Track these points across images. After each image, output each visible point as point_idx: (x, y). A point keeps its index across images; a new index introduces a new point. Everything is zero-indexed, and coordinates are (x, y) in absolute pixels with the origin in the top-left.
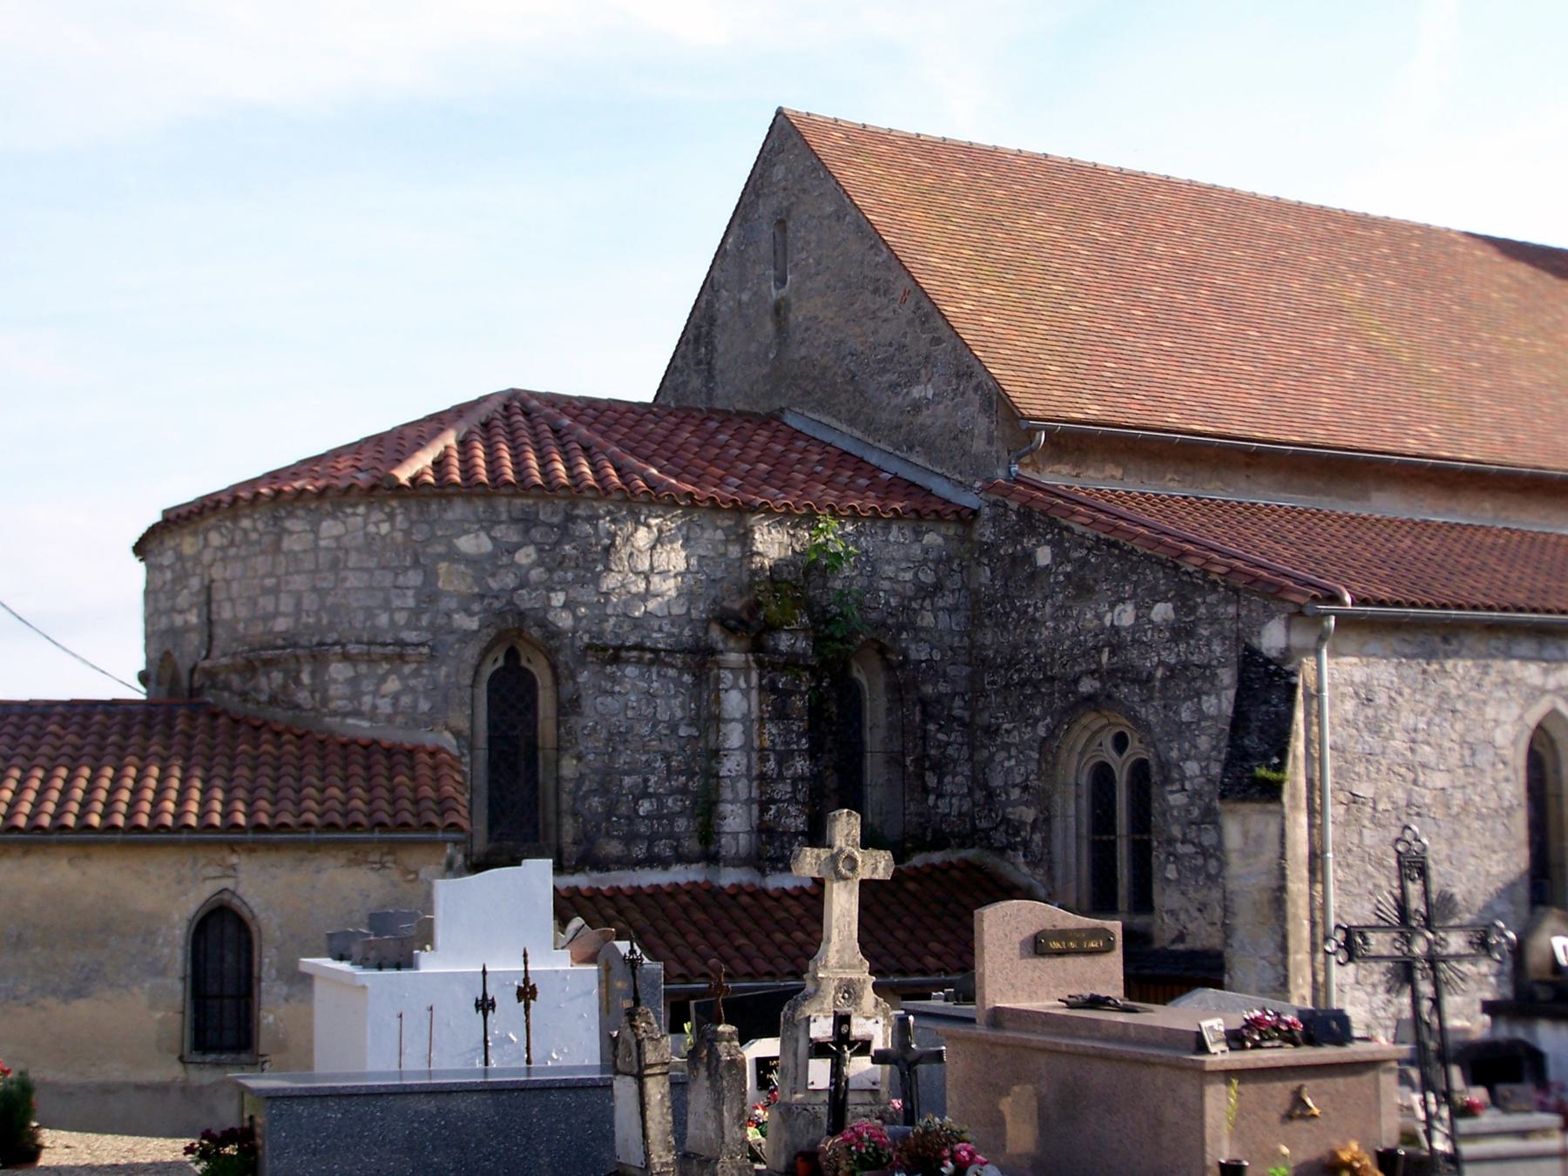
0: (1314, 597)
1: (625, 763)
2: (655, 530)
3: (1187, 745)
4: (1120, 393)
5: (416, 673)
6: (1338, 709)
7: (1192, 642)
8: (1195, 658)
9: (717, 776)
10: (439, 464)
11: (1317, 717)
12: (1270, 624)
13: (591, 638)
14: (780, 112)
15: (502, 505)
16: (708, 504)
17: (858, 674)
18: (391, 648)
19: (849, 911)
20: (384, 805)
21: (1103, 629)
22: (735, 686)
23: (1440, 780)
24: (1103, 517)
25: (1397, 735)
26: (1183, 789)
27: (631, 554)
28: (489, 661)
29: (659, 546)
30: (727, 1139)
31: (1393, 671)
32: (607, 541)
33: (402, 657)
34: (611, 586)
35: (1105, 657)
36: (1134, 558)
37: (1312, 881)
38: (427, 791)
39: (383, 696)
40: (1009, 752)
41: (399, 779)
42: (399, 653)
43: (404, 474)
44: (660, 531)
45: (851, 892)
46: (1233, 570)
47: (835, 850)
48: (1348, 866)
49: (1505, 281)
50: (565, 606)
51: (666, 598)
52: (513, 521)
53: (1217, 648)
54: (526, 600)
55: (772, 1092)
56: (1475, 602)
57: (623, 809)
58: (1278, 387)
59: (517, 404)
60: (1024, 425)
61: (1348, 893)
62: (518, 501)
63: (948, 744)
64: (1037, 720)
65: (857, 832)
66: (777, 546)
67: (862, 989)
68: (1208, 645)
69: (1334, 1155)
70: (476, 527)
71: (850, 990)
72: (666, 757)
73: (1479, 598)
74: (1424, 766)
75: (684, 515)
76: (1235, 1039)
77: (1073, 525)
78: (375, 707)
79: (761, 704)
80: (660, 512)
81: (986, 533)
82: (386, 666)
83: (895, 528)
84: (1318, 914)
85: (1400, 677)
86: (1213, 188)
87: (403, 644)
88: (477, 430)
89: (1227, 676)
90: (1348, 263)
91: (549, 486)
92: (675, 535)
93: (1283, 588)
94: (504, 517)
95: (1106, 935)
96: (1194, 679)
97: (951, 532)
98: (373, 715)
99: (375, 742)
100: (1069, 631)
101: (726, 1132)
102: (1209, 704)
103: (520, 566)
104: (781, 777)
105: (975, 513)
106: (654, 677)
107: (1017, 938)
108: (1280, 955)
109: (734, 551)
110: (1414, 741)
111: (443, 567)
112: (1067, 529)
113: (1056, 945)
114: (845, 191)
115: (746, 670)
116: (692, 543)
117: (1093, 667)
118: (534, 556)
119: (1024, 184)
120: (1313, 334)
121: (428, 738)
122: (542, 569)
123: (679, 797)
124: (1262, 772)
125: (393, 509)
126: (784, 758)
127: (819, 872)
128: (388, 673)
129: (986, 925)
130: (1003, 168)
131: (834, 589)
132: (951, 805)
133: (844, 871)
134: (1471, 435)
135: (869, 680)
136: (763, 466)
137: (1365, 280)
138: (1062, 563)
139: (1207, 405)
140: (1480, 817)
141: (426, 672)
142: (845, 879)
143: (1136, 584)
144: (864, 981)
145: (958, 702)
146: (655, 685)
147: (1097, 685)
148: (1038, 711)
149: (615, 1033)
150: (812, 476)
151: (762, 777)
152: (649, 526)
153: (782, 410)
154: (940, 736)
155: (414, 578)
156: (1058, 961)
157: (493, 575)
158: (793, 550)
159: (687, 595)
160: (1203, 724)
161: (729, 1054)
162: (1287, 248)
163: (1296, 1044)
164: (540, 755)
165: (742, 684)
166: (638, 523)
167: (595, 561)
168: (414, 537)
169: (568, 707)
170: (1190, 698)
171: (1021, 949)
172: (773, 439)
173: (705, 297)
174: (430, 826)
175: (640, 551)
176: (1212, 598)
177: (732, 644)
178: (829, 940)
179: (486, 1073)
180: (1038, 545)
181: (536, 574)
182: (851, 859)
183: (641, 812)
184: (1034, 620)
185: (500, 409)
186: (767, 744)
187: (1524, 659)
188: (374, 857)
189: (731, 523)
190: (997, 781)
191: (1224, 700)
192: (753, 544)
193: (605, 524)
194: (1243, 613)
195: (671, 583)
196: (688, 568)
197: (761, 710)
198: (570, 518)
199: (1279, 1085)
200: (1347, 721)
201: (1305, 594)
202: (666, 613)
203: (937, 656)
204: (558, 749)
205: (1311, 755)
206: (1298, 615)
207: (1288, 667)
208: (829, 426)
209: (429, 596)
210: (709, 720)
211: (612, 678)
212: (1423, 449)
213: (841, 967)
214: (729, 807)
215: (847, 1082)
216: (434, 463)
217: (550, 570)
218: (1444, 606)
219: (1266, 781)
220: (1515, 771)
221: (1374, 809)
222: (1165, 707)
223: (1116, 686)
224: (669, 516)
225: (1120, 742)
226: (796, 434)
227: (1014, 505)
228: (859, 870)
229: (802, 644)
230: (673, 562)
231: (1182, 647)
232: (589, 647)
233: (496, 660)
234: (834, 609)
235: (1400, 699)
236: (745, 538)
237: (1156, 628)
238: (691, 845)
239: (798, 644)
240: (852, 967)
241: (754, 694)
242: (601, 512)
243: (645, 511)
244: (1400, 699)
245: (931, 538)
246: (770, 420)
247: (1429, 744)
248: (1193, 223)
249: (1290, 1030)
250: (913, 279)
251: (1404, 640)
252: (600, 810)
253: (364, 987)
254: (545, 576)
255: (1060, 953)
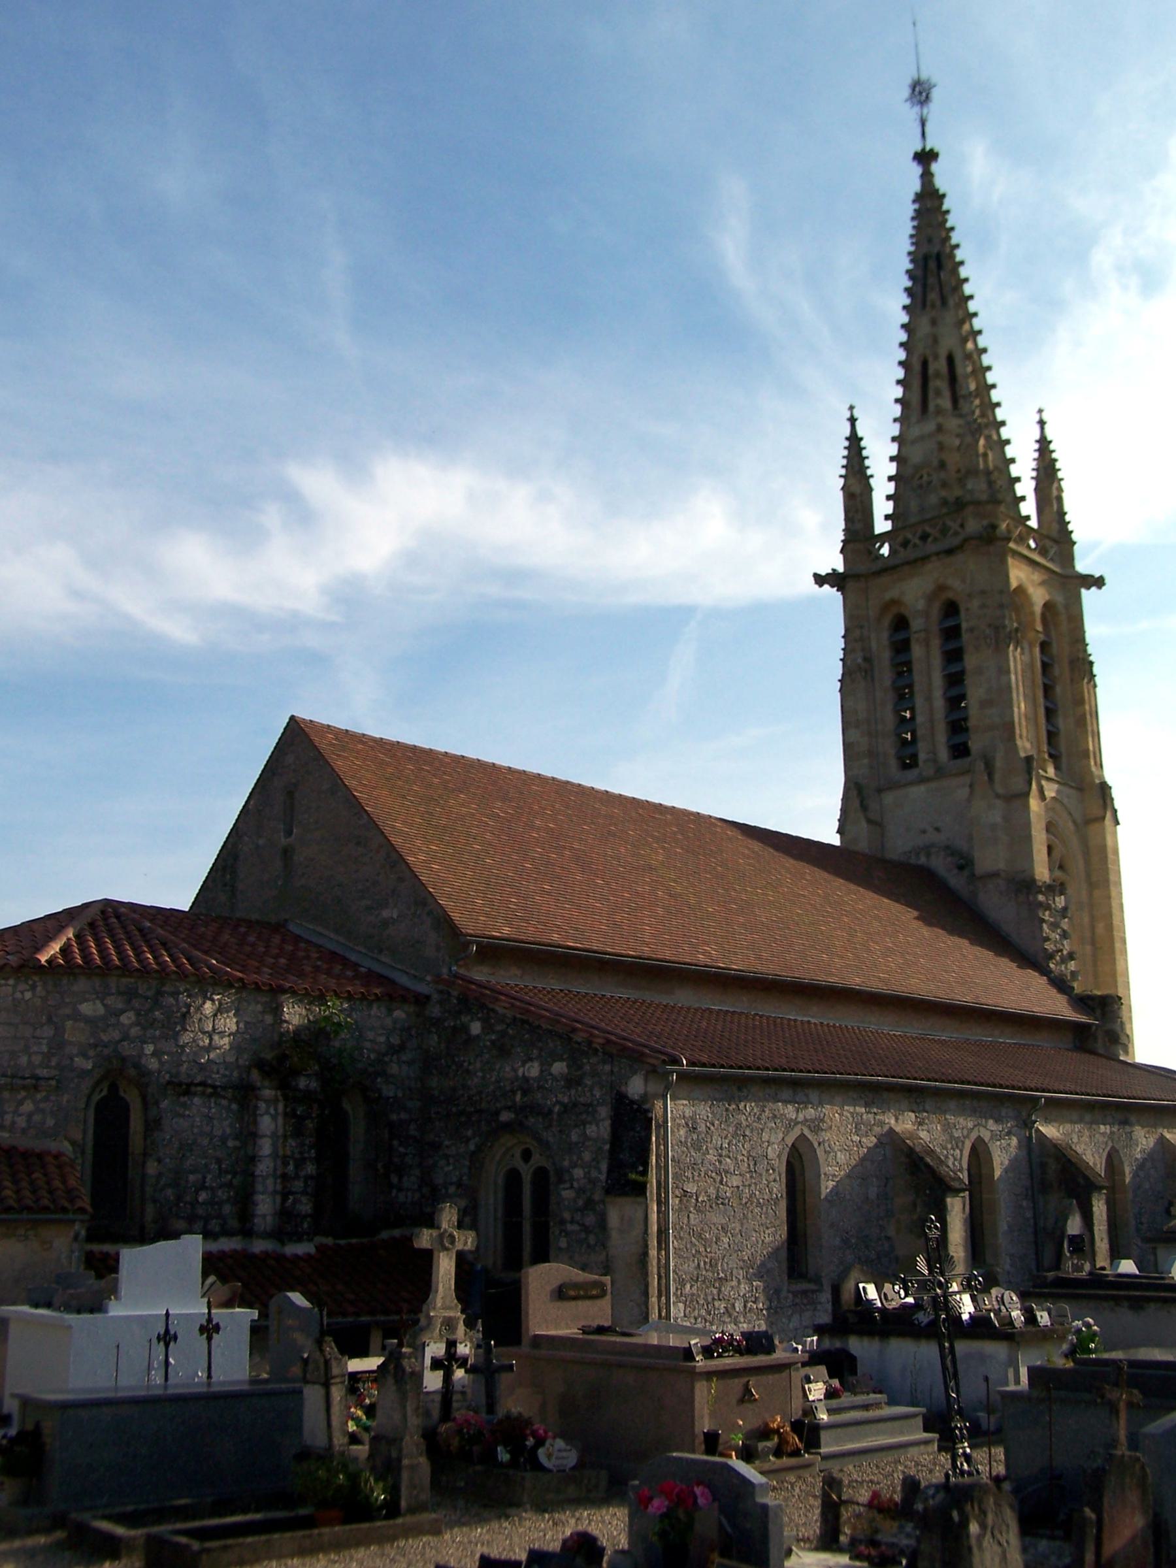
0: (664, 1061)
1: (191, 1165)
2: (217, 1003)
3: (575, 1158)
4: (522, 919)
5: (46, 1099)
6: (676, 1134)
7: (580, 1088)
8: (582, 1100)
9: (253, 1175)
10: (65, 950)
11: (663, 1140)
12: (635, 1077)
13: (171, 1077)
14: (292, 718)
15: (113, 982)
16: (253, 986)
17: (347, 1106)
18: (29, 1080)
19: (450, 1271)
20: (28, 1193)
21: (517, 1078)
22: (267, 1113)
23: (735, 1181)
24: (518, 1003)
25: (711, 1152)
26: (572, 1187)
27: (200, 1020)
28: (98, 1090)
29: (219, 1014)
30: (409, 1424)
31: (708, 1109)
32: (184, 1010)
33: (36, 1088)
34: (186, 1041)
35: (518, 1097)
36: (541, 1032)
37: (659, 1249)
38: (57, 1183)
39: (20, 1115)
40: (448, 1161)
41: (35, 1175)
42: (35, 1084)
43: (43, 958)
44: (220, 1004)
45: (451, 1259)
46: (609, 1041)
47: (442, 1230)
48: (681, 1238)
49: (746, 852)
50: (154, 1054)
51: (223, 1050)
52: (120, 993)
53: (598, 1094)
54: (127, 1049)
55: (359, 1396)
56: (758, 1065)
57: (188, 1198)
58: (618, 918)
59: (110, 910)
60: (462, 939)
61: (680, 1257)
62: (124, 980)
63: (406, 1154)
64: (468, 1140)
65: (455, 1218)
66: (297, 1016)
67: (457, 1323)
68: (591, 1090)
69: (767, 1425)
70: (94, 996)
71: (449, 1324)
72: (219, 1161)
73: (759, 1063)
74: (727, 1172)
75: (236, 993)
76: (707, 1352)
77: (497, 1008)
78: (13, 1123)
79: (284, 1125)
80: (221, 991)
81: (435, 1011)
82: (23, 1093)
83: (375, 1006)
84: (663, 1271)
85: (712, 1113)
86: (568, 782)
87: (38, 1078)
88: (86, 927)
89: (604, 1112)
90: (653, 837)
91: (144, 971)
92: (230, 1007)
93: (643, 1054)
94: (114, 991)
95: (601, 1285)
96: (581, 1113)
97: (412, 1010)
98: (12, 1128)
99: (14, 1148)
100: (493, 1079)
101: (409, 1419)
102: (591, 1130)
103: (123, 1025)
104: (297, 1177)
105: (428, 997)
106: (213, 1105)
107: (549, 1288)
108: (643, 1298)
109: (269, 1019)
110: (721, 1156)
111: (69, 1023)
112: (493, 1010)
113: (572, 1293)
114: (338, 775)
115: (276, 1101)
116: (241, 1012)
117: (509, 1104)
118: (133, 1018)
119: (450, 775)
120: (636, 883)
121: (53, 1146)
122: (139, 1028)
123: (226, 1189)
124: (633, 1176)
125: (35, 982)
126: (300, 1163)
127: (431, 1245)
128: (25, 1098)
129: (530, 1279)
130: (437, 764)
131: (334, 1047)
132: (407, 1197)
133: (447, 1245)
134: (736, 953)
135: (354, 1109)
136: (283, 961)
137: (664, 848)
138: (488, 1033)
139: (576, 929)
140: (759, 1205)
141: (53, 1098)
142: (447, 1249)
143: (541, 1049)
144: (458, 1318)
145: (412, 1126)
146: (213, 1110)
147: (513, 1116)
148: (470, 1133)
149: (306, 1355)
150: (317, 969)
151: (284, 1176)
152: (213, 1000)
153: (286, 920)
154: (402, 1149)
155: (48, 1032)
156: (573, 1303)
157: (104, 1031)
158: (309, 1020)
159: (236, 1047)
160: (587, 1143)
161: (410, 1367)
162: (615, 825)
163: (741, 1354)
164: (130, 1158)
165: (272, 1111)
166: (205, 998)
167: (176, 1024)
168: (49, 1003)
169: (152, 1125)
170: (576, 1126)
171: (551, 1296)
172: (283, 941)
173: (231, 840)
174: (64, 1210)
175: (206, 1017)
176: (593, 1060)
177: (266, 1083)
178: (437, 1291)
179: (209, 1384)
180: (472, 1020)
181: (134, 1031)
182: (452, 1237)
183: (200, 1199)
184: (468, 1071)
185: (99, 913)
186: (289, 1153)
187: (786, 1102)
188: (21, 1231)
189: (268, 1000)
190: (439, 1180)
191: (601, 1127)
192: (282, 1015)
193: (183, 998)
194: (616, 1070)
195: (226, 1040)
196: (237, 1030)
197: (285, 1130)
198: (159, 993)
199: (736, 1380)
200: (681, 1142)
201: (657, 1058)
202: (222, 1061)
203: (400, 1095)
204: (145, 1154)
205: (659, 1164)
206: (653, 1072)
207: (646, 1106)
208: (321, 934)
209: (57, 1044)
210: (249, 1135)
211: (184, 1105)
212: (709, 962)
213: (443, 1309)
214: (261, 1197)
215: (453, 1387)
216: (60, 950)
217: (144, 1028)
218: (741, 1068)
219: (635, 1182)
220: (780, 1175)
221: (697, 1200)
222: (560, 1131)
223: (526, 1117)
224: (226, 994)
225: (527, 1155)
226: (297, 939)
227: (455, 993)
228: (457, 1244)
229: (314, 1085)
230: (228, 1025)
231: (573, 1092)
232: (169, 1083)
233: (102, 1090)
234: (334, 1061)
235: (712, 1128)
236: (277, 1011)
237: (555, 1079)
238: (234, 1223)
239: (311, 1084)
240: (450, 1308)
241: (280, 1120)
242: (181, 989)
243: (211, 989)
244: (712, 1128)
245: (398, 1014)
246: (278, 928)
247: (729, 1157)
248: (557, 806)
249: (739, 1345)
250: (386, 837)
251: (716, 1089)
252: (172, 1198)
253: (70, 1327)
254: (140, 1033)
255: (575, 1298)
